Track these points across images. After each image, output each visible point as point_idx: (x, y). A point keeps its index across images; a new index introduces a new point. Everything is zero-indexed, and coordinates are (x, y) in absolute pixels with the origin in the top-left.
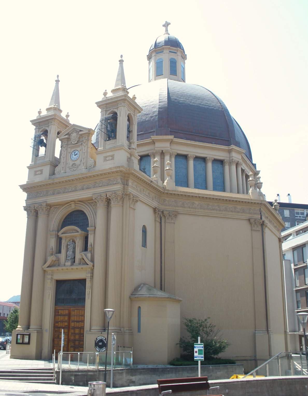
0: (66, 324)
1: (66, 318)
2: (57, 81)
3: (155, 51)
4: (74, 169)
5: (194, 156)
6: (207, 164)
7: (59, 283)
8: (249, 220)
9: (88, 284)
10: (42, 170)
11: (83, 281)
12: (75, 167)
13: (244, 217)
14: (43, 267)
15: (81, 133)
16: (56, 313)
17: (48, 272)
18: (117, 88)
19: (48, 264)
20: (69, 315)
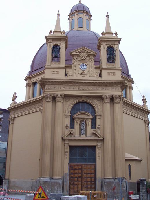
0: (80, 175)
1: (80, 171)
2: (59, 15)
11: (94, 148)
16: (71, 168)
20: (82, 170)
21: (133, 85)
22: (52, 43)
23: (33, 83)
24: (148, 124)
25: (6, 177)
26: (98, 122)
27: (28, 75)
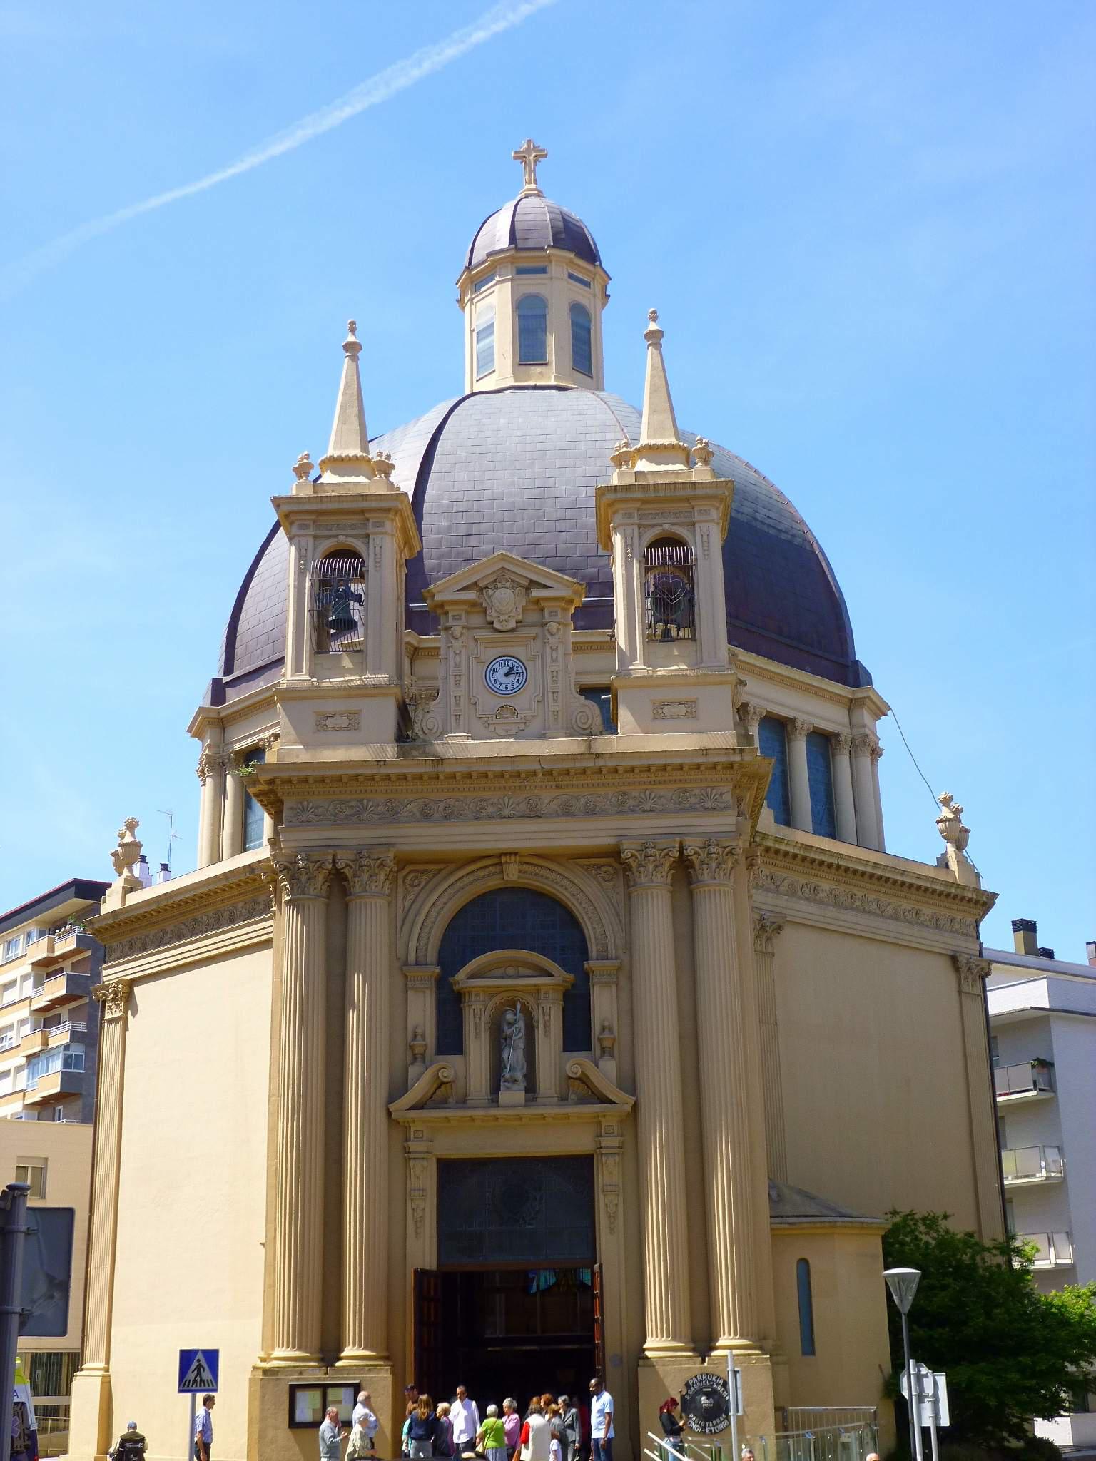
3: (512, 260)
4: (507, 727)
5: (762, 710)
6: (793, 744)
7: (450, 1171)
8: (954, 959)
9: (607, 1175)
10: (358, 713)
12: (512, 720)
13: (942, 946)
14: (392, 1107)
15: (536, 593)
17: (412, 1129)
18: (659, 442)
19: (418, 1090)
21: (884, 730)
22: (315, 537)
23: (237, 753)
24: (983, 979)
25: (987, 985)
26: (603, 1005)
27: (208, 704)
